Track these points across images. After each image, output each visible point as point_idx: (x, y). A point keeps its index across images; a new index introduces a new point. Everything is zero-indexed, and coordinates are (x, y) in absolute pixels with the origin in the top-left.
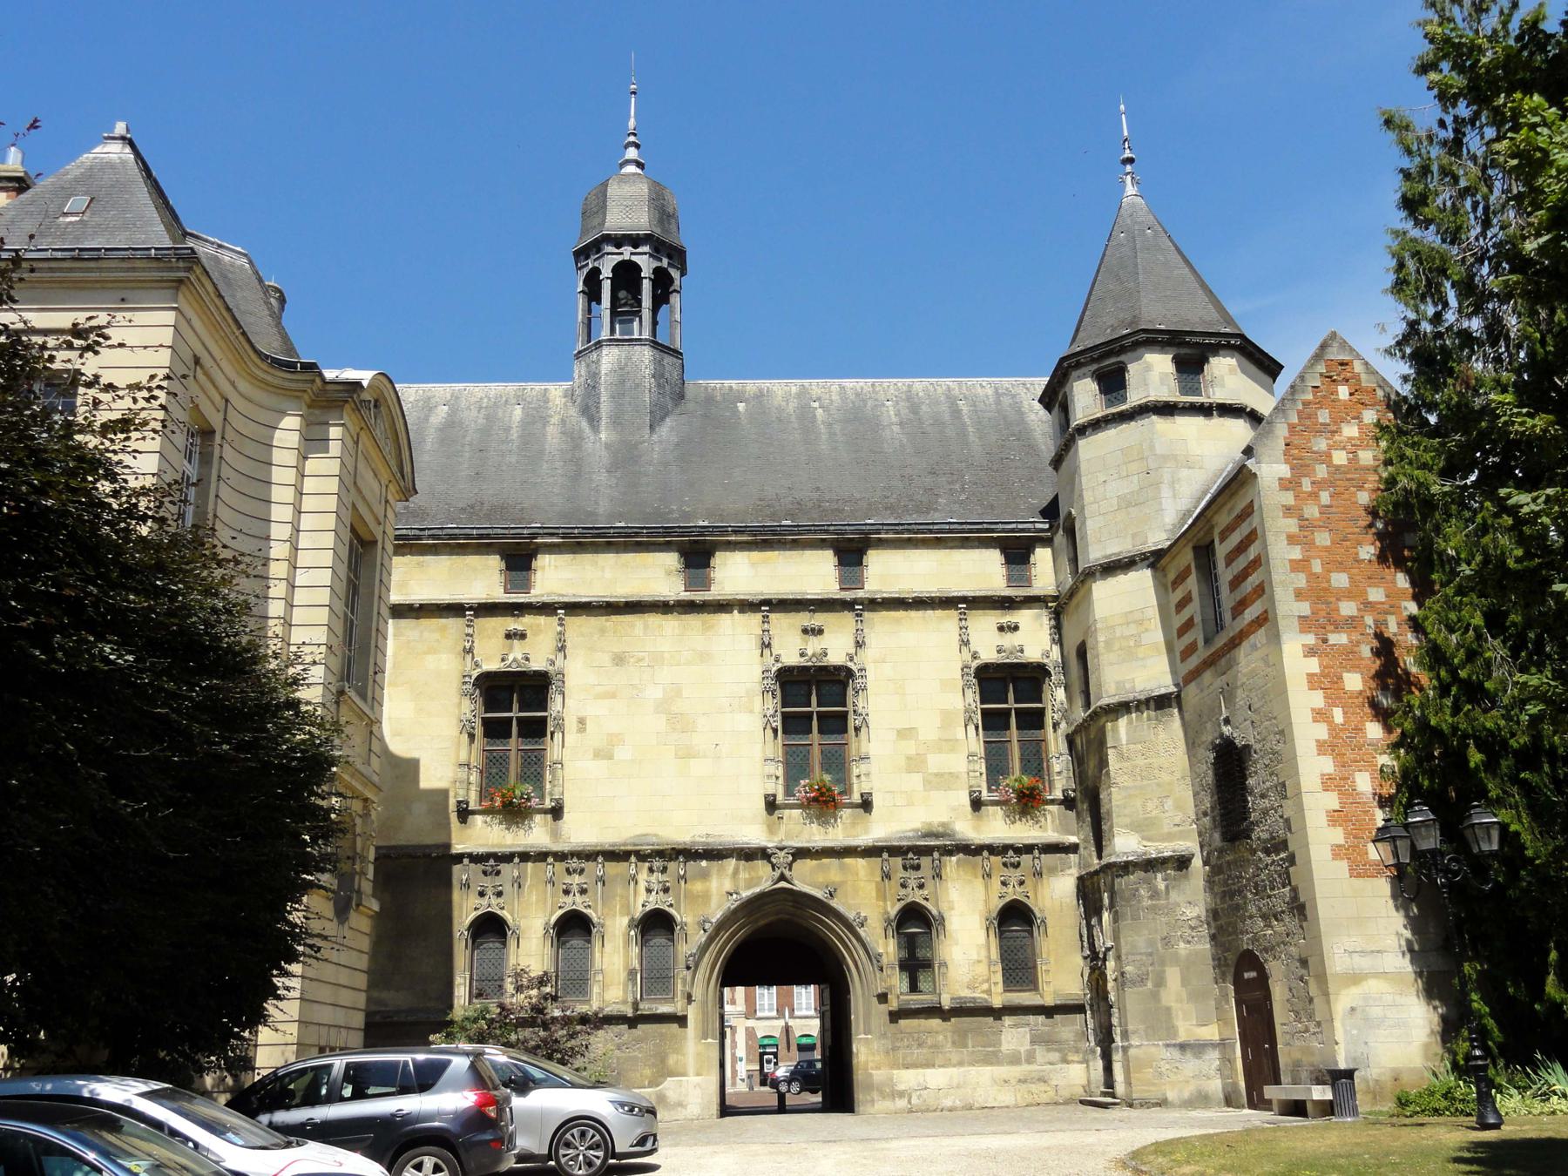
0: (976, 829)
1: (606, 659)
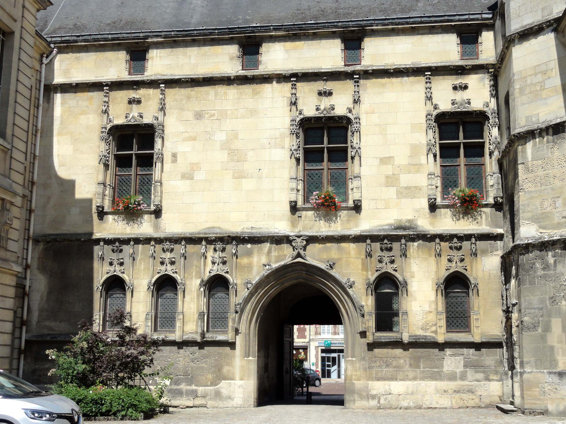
0: (432, 224)
1: (190, 115)
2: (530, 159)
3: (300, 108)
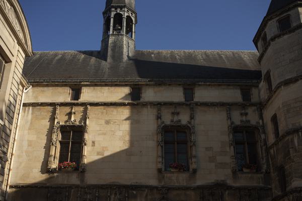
1: (103, 122)
3: (163, 120)
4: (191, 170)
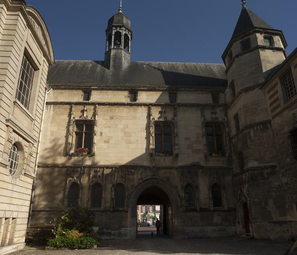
1: (108, 118)
2: (252, 136)
4: (174, 154)
